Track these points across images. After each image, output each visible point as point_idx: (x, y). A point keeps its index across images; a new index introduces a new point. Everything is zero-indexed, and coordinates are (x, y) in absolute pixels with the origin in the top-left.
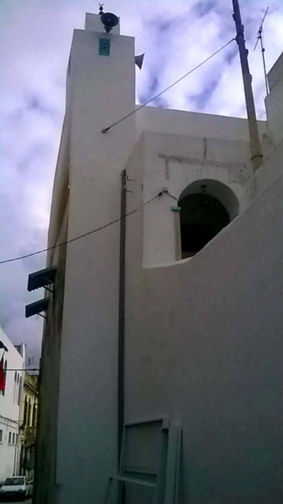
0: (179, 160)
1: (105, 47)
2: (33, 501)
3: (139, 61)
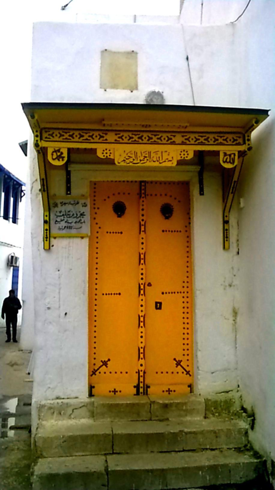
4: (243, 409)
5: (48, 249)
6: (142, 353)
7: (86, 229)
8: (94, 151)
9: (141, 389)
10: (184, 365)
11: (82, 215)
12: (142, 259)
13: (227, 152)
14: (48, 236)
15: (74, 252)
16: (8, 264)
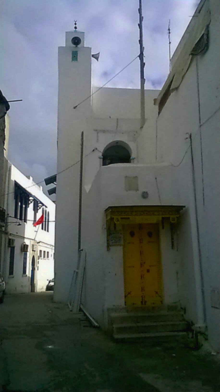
0: (104, 131)
1: (75, 56)
3: (96, 57)
4: (182, 308)
6: (143, 289)
7: (122, 242)
9: (143, 302)
12: (141, 253)
13: (173, 217)
14: (108, 246)
15: (118, 252)
16: (21, 249)
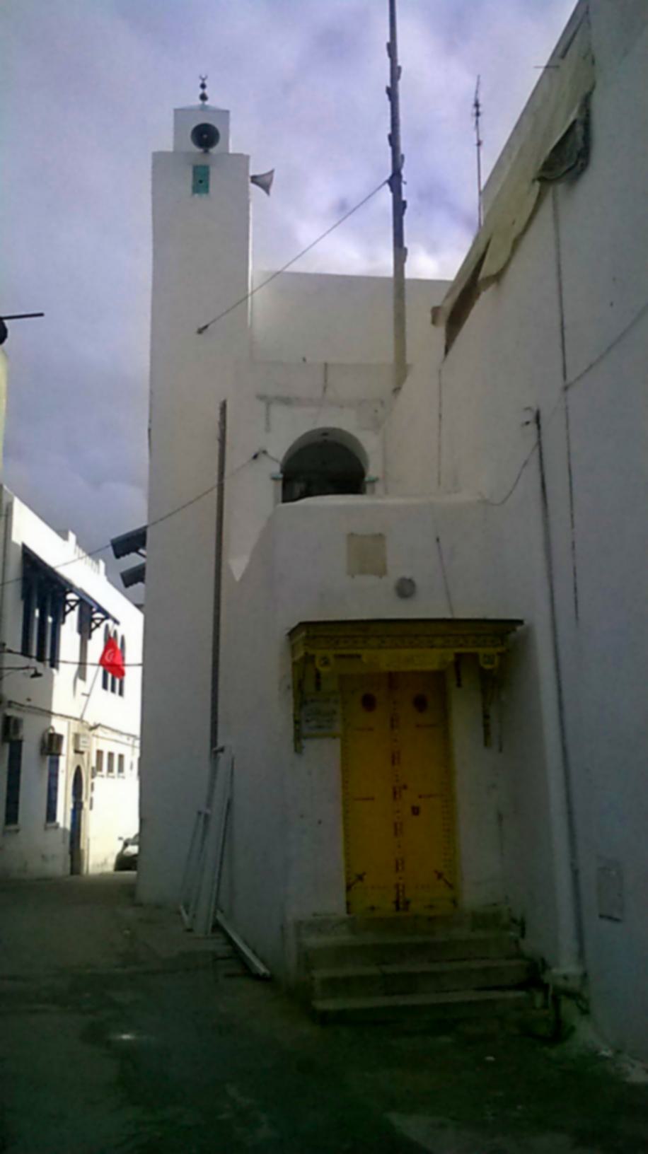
0: (287, 401)
1: (201, 181)
2: (74, 532)
4: (514, 921)
5: (298, 750)
7: (338, 727)
8: (359, 656)
10: (447, 878)
11: (334, 712)
12: (395, 759)
14: (298, 737)
15: (325, 754)
